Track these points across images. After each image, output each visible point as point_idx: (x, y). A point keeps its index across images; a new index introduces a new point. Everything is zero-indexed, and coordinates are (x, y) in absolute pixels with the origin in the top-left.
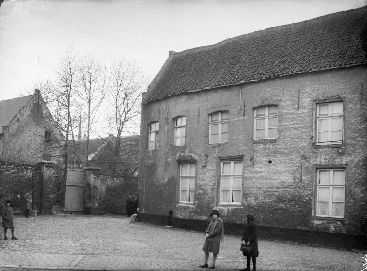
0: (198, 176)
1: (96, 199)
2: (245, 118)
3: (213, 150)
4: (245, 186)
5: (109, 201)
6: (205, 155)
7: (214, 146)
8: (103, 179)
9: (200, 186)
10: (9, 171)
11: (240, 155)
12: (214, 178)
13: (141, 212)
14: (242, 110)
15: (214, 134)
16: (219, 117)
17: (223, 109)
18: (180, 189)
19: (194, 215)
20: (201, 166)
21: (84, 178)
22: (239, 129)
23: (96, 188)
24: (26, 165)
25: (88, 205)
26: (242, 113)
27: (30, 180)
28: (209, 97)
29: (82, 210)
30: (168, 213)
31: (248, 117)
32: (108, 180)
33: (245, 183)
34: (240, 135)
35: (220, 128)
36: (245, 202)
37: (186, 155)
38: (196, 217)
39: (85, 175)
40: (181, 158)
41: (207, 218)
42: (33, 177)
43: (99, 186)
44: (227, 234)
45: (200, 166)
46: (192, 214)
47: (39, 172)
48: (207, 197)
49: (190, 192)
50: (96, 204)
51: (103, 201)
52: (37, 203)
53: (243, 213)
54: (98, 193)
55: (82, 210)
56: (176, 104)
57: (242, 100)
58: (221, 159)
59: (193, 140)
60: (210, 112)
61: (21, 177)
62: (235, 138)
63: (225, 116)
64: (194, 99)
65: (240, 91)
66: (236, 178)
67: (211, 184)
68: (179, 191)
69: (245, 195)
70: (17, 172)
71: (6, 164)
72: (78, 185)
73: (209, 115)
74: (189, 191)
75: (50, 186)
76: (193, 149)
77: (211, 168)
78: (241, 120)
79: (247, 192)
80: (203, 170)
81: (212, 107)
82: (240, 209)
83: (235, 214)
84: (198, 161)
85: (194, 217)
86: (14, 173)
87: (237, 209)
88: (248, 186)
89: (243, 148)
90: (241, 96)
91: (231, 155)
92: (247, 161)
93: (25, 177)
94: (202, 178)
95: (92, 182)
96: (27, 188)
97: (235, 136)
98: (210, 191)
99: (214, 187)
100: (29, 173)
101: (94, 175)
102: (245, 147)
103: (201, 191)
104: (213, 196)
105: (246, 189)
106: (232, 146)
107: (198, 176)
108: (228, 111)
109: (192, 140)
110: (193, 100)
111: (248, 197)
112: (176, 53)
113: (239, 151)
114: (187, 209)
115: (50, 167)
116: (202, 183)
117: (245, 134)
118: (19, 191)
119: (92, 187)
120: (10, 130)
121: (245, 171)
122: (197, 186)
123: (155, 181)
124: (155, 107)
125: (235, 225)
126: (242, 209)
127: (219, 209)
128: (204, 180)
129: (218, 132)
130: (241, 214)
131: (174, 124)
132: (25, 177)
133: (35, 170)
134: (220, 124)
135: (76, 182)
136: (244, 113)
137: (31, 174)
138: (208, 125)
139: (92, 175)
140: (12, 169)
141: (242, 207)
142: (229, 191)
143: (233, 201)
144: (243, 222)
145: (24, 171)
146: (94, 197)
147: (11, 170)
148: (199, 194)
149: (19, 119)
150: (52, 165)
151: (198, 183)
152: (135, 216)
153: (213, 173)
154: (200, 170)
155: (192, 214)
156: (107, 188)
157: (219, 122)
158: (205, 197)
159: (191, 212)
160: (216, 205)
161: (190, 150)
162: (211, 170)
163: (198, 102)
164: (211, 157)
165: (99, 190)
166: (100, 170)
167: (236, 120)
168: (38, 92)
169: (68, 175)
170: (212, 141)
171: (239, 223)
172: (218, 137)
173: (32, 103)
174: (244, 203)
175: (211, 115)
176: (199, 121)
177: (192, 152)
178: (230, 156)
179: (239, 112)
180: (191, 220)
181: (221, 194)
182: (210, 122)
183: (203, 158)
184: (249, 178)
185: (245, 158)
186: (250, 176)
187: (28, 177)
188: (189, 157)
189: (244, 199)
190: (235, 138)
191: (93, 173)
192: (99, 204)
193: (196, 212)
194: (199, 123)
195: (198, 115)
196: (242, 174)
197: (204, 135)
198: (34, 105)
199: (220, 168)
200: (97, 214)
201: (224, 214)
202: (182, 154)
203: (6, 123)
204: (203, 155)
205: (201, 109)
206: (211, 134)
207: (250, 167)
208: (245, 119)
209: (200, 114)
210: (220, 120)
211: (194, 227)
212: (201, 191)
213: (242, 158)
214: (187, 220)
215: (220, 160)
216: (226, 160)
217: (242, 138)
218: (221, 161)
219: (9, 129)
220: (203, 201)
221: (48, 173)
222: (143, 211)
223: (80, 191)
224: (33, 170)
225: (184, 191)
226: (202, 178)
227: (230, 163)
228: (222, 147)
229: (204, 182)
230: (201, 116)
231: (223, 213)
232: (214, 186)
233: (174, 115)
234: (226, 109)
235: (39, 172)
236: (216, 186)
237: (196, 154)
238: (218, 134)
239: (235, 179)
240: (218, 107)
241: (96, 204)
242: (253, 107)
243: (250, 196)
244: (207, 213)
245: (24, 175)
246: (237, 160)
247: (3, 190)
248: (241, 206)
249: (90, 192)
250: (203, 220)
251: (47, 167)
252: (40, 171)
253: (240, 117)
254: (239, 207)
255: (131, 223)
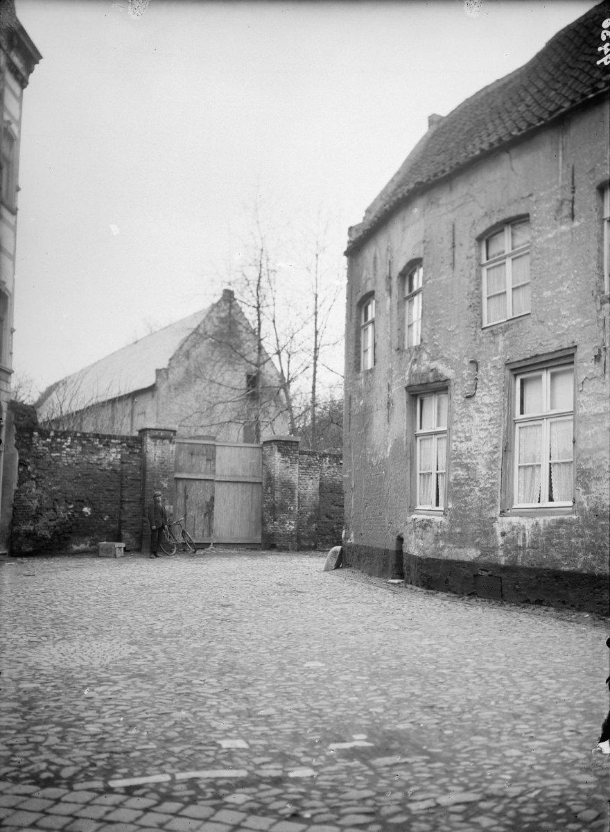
0: (454, 428)
1: (291, 512)
2: (576, 224)
3: (491, 342)
4: (581, 446)
5: (327, 516)
6: (471, 362)
7: (493, 331)
8: (310, 465)
9: (459, 456)
10: (59, 450)
11: (566, 346)
12: (495, 430)
13: (349, 541)
14: (566, 203)
15: (494, 296)
16: (504, 243)
17: (512, 212)
18: (418, 472)
19: (444, 547)
20: (460, 397)
21: (263, 464)
22: (560, 264)
23: (288, 485)
24: (104, 436)
25: (270, 528)
26: (566, 211)
27: (115, 471)
28: (475, 186)
29: (258, 539)
30: (395, 541)
31: (582, 220)
32: (325, 466)
33: (581, 437)
34: (561, 282)
35: (510, 273)
36: (583, 498)
37: (423, 369)
38: (451, 552)
39: (264, 457)
40: (414, 382)
41: (479, 553)
42: (123, 463)
43: (296, 481)
44: (533, 603)
45: (457, 393)
46: (441, 544)
47: (138, 451)
48: (477, 489)
49: (440, 477)
50: (290, 524)
51: (311, 517)
52: (133, 525)
53: (580, 536)
54: (293, 497)
55: (259, 539)
56: (404, 230)
57: (565, 171)
58: (513, 367)
59: (439, 323)
60: (481, 229)
61: (90, 465)
62: (547, 294)
63: (523, 236)
64: (441, 202)
65: (557, 143)
66: (556, 422)
67: (488, 448)
68: (416, 477)
69: (583, 477)
70: (81, 453)
71: (52, 434)
72: (248, 480)
73: (479, 239)
74: (437, 474)
75: (166, 485)
76: (440, 347)
77: (487, 400)
78: (563, 234)
79: (590, 465)
80: (467, 407)
81: (486, 214)
82: (570, 524)
83: (555, 541)
84: (452, 383)
85: (446, 551)
86: (73, 456)
87: (561, 522)
88: (590, 447)
89: (574, 323)
90: (561, 158)
91: (540, 351)
92: (585, 365)
93: (101, 464)
94: (463, 432)
95: (278, 472)
96: (108, 490)
97: (548, 290)
98: (484, 472)
99: (495, 456)
100: (113, 455)
101: (283, 456)
102: (579, 320)
103: (461, 473)
104: (493, 484)
105: (585, 457)
106: (542, 322)
107: (454, 428)
108: (528, 215)
109: (439, 323)
110: (438, 206)
111: (594, 482)
112: (442, 118)
113: (559, 335)
114: (428, 528)
115: (163, 438)
116: (463, 447)
117: (577, 275)
118: (88, 499)
119: (278, 485)
120: (171, 376)
121: (582, 398)
122: (455, 459)
123: (371, 456)
124: (369, 253)
125: (557, 575)
126: (577, 521)
127: (510, 523)
128: (468, 439)
129: (505, 287)
130: (573, 540)
131: (404, 290)
132: (101, 464)
133: (129, 446)
134: (509, 261)
135: (240, 472)
136: (572, 209)
137: (119, 456)
138: (479, 272)
139: (278, 455)
140: (68, 447)
141: (575, 517)
142: (540, 465)
143: (551, 499)
144: (579, 566)
145: (99, 450)
146: (283, 508)
147: (64, 449)
148: (458, 483)
149: (188, 351)
150: (166, 432)
151: (454, 448)
152: (335, 552)
153: (492, 415)
154: (457, 409)
155: (441, 544)
156: (321, 485)
157: (505, 258)
158: (471, 490)
159: (437, 538)
160: (502, 513)
161: (432, 351)
162: (487, 405)
163: (450, 208)
164: (486, 366)
165: (296, 492)
166: (297, 442)
167: (550, 236)
168: (229, 296)
169: (220, 458)
170: (492, 315)
171: (567, 569)
172: (506, 301)
173: (217, 318)
174: (581, 503)
175: (486, 238)
176: (453, 265)
177: (437, 359)
178: (537, 356)
179: (559, 211)
180: (439, 561)
181: (517, 478)
182: (484, 261)
183: (465, 372)
184: (593, 419)
185: (580, 355)
186: (596, 411)
187: (110, 464)
188: (431, 375)
189: (582, 490)
190: (547, 294)
191: (279, 451)
192: (299, 526)
193: (450, 537)
194: (453, 268)
195: (450, 245)
196: (572, 410)
197: (467, 303)
198: (222, 320)
199: (510, 397)
200: (293, 550)
201: (524, 540)
202: (415, 367)
203: (164, 364)
204: (466, 361)
205: (459, 227)
206: (488, 298)
207: (594, 381)
208: (575, 229)
209: (456, 243)
210: (508, 250)
211: (447, 581)
212: (461, 473)
213: (573, 355)
214: (428, 559)
215: (512, 370)
216: (524, 369)
217: (569, 292)
218: (515, 376)
219: (167, 375)
220: (465, 502)
221: (159, 452)
222: (352, 541)
223: (252, 496)
224: (123, 447)
225: (426, 476)
226: (463, 432)
227: (540, 377)
228: (515, 329)
229: (470, 444)
230: (458, 247)
231: (521, 536)
232: (495, 453)
233: (400, 265)
234: (522, 211)
235: (138, 451)
236: (500, 454)
237: (447, 361)
238: (505, 293)
239: (554, 428)
240: (499, 211)
241: (290, 524)
242: (598, 183)
243: (598, 479)
244: (478, 540)
245: (99, 459)
246: (562, 365)
247: (44, 496)
248: (572, 513)
249: (273, 497)
250: (467, 559)
251: (154, 438)
252: (141, 450)
253: (561, 224)
254: (566, 517)
255: (326, 570)
